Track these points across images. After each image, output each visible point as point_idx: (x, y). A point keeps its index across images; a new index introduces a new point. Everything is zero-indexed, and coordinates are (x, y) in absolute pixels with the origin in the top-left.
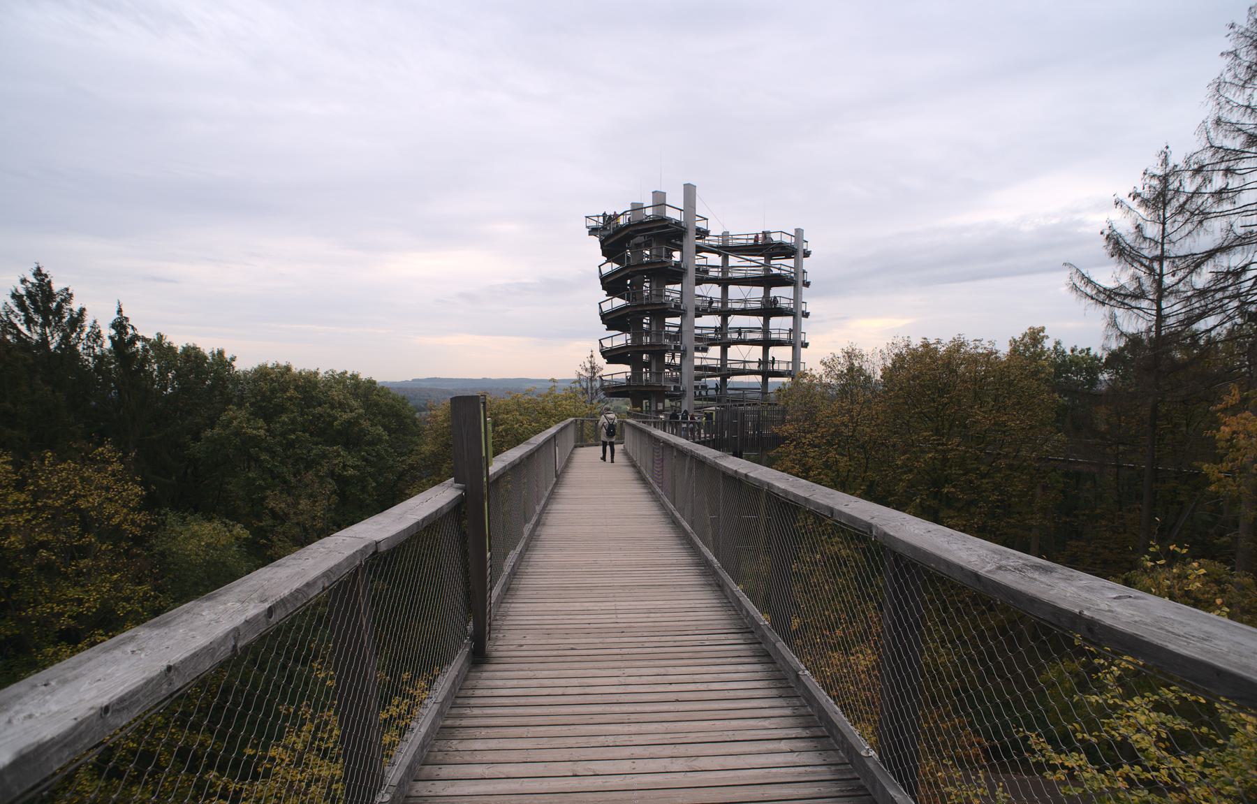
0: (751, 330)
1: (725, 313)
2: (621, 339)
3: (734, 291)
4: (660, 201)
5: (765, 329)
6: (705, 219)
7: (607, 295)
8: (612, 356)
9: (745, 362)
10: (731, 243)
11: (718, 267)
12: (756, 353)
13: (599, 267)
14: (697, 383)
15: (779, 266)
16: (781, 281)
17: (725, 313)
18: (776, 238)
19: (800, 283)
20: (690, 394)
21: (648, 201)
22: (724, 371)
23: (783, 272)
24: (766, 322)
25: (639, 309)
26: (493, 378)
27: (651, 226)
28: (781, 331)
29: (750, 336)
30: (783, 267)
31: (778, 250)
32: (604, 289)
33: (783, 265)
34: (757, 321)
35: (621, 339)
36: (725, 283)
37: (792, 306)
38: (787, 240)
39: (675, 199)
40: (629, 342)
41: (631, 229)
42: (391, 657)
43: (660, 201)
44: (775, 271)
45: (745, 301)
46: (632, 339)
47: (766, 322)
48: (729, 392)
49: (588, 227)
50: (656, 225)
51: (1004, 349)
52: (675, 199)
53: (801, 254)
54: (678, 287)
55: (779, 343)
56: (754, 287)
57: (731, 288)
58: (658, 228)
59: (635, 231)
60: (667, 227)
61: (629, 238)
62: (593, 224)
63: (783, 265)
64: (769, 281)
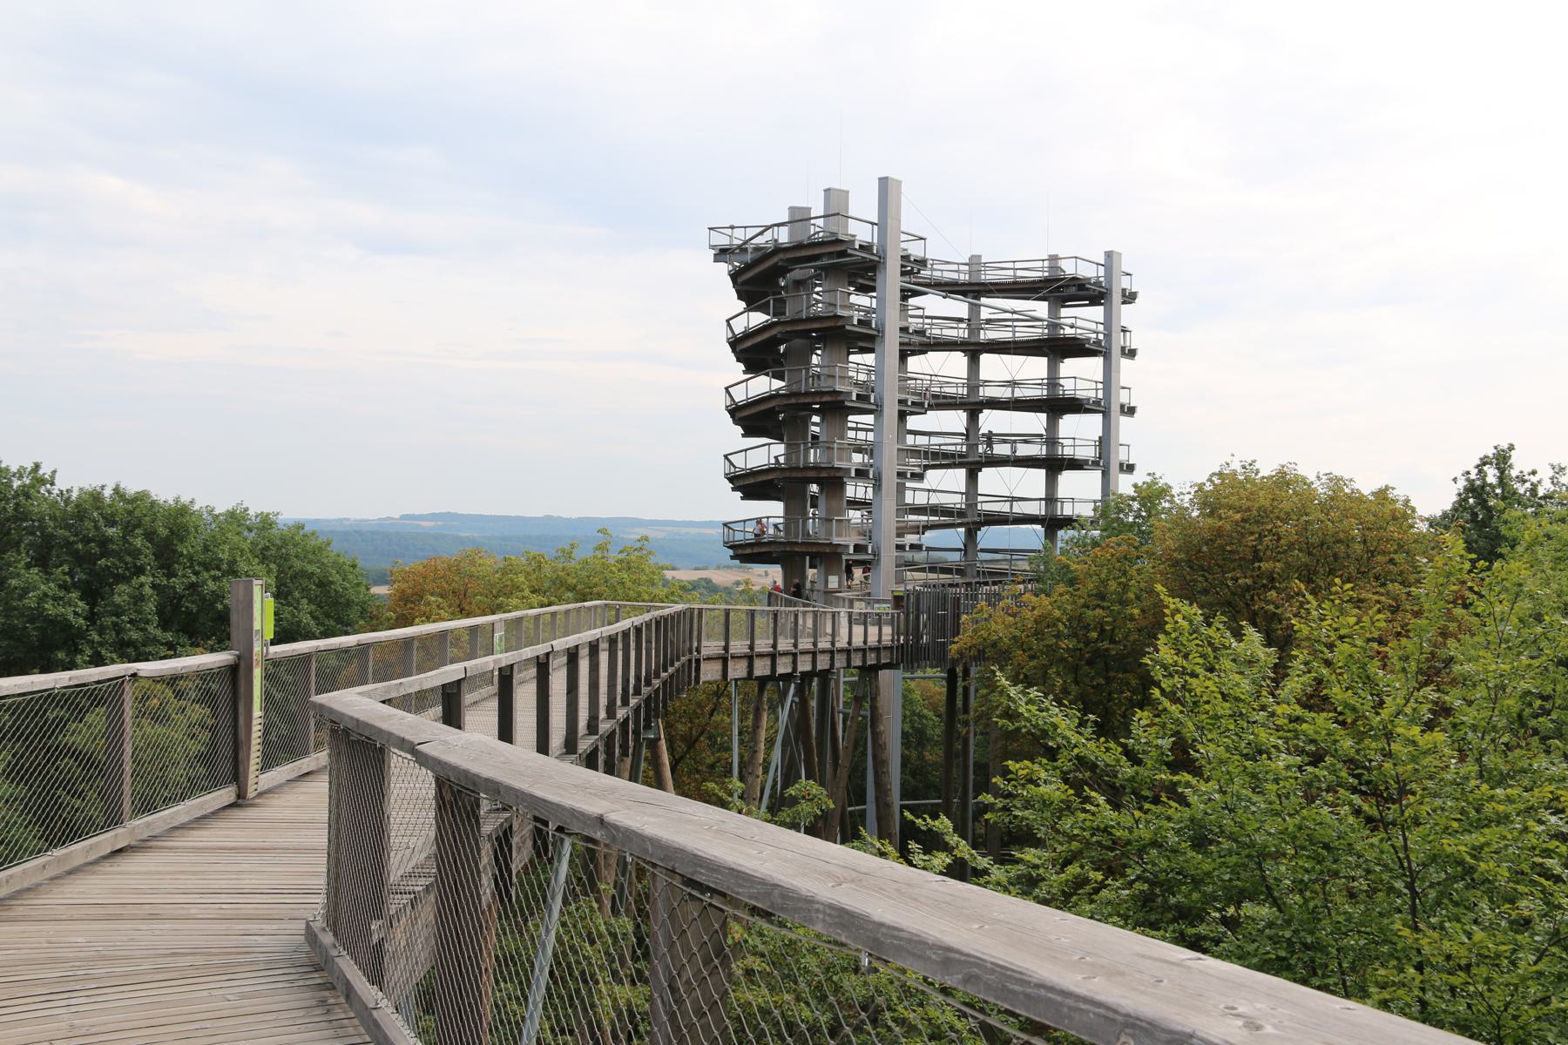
0: (1027, 439)
1: (974, 408)
2: (765, 453)
3: (994, 367)
4: (836, 204)
5: (1051, 440)
6: (921, 239)
7: (745, 372)
8: (751, 485)
9: (1013, 499)
10: (989, 276)
11: (960, 320)
12: (1032, 482)
13: (728, 321)
14: (899, 541)
15: (1073, 320)
16: (1077, 348)
17: (974, 408)
18: (1069, 268)
19: (1116, 351)
20: (888, 558)
21: (818, 209)
22: (972, 519)
23: (1079, 331)
24: (1052, 425)
25: (793, 401)
26: (564, 516)
27: (817, 251)
28: (1077, 442)
29: (1024, 450)
30: (1079, 323)
31: (1073, 290)
32: (738, 360)
33: (1082, 319)
34: (1035, 422)
35: (765, 453)
36: (974, 350)
37: (1100, 395)
38: (1087, 272)
39: (863, 206)
40: (782, 460)
41: (781, 256)
42: (71, 831)
43: (836, 204)
44: (1068, 331)
45: (1013, 384)
46: (787, 455)
47: (1052, 425)
48: (983, 556)
49: (712, 247)
50: (823, 251)
51: (1321, 490)
52: (863, 206)
53: (1117, 297)
54: (869, 359)
55: (1076, 464)
56: (1029, 357)
57: (985, 358)
58: (830, 255)
59: (789, 260)
60: (843, 254)
61: (781, 271)
62: (723, 241)
63: (1082, 319)
64: (1058, 347)
